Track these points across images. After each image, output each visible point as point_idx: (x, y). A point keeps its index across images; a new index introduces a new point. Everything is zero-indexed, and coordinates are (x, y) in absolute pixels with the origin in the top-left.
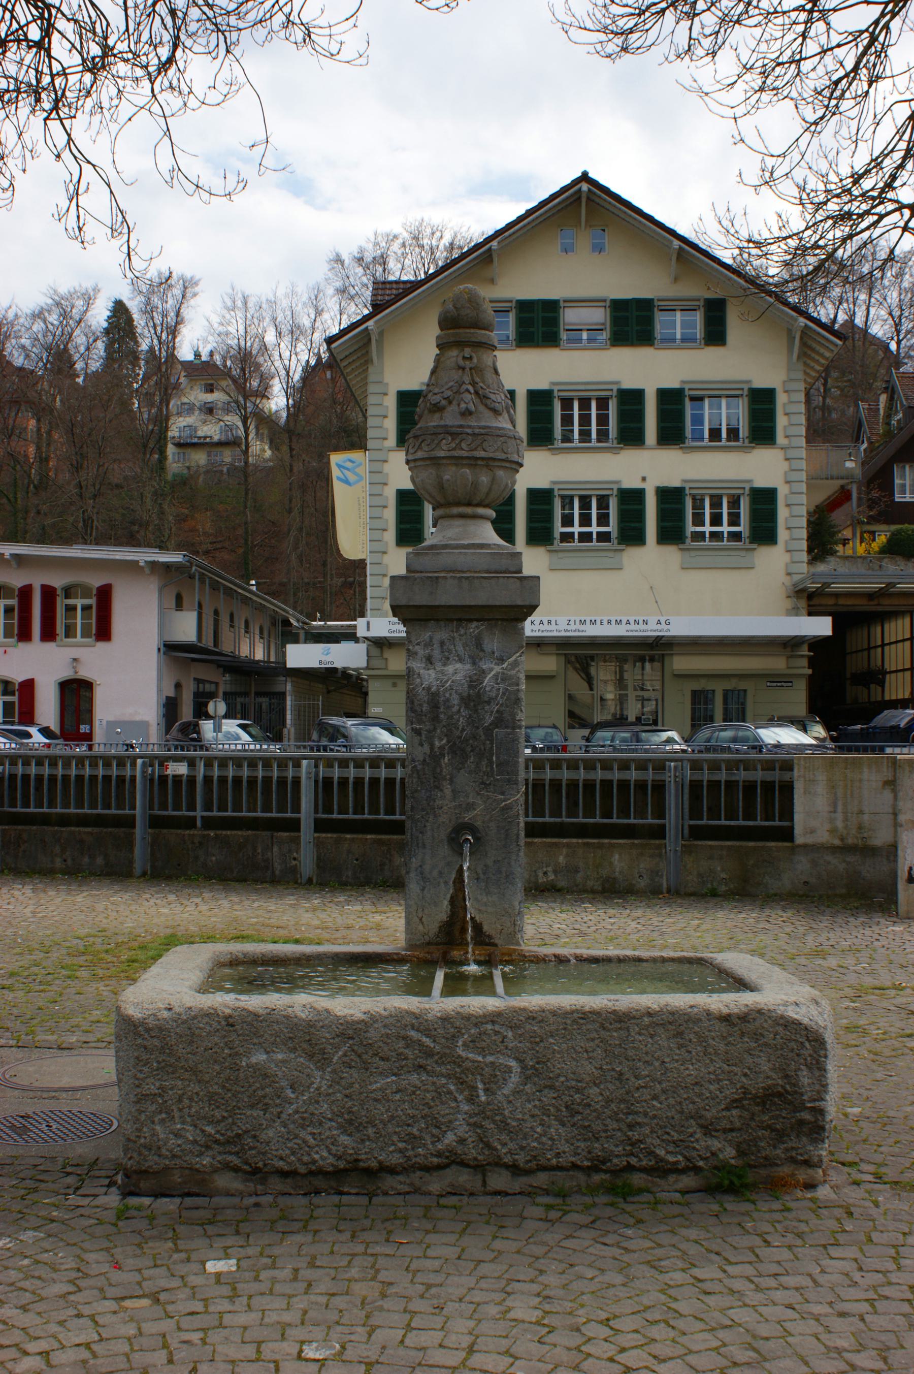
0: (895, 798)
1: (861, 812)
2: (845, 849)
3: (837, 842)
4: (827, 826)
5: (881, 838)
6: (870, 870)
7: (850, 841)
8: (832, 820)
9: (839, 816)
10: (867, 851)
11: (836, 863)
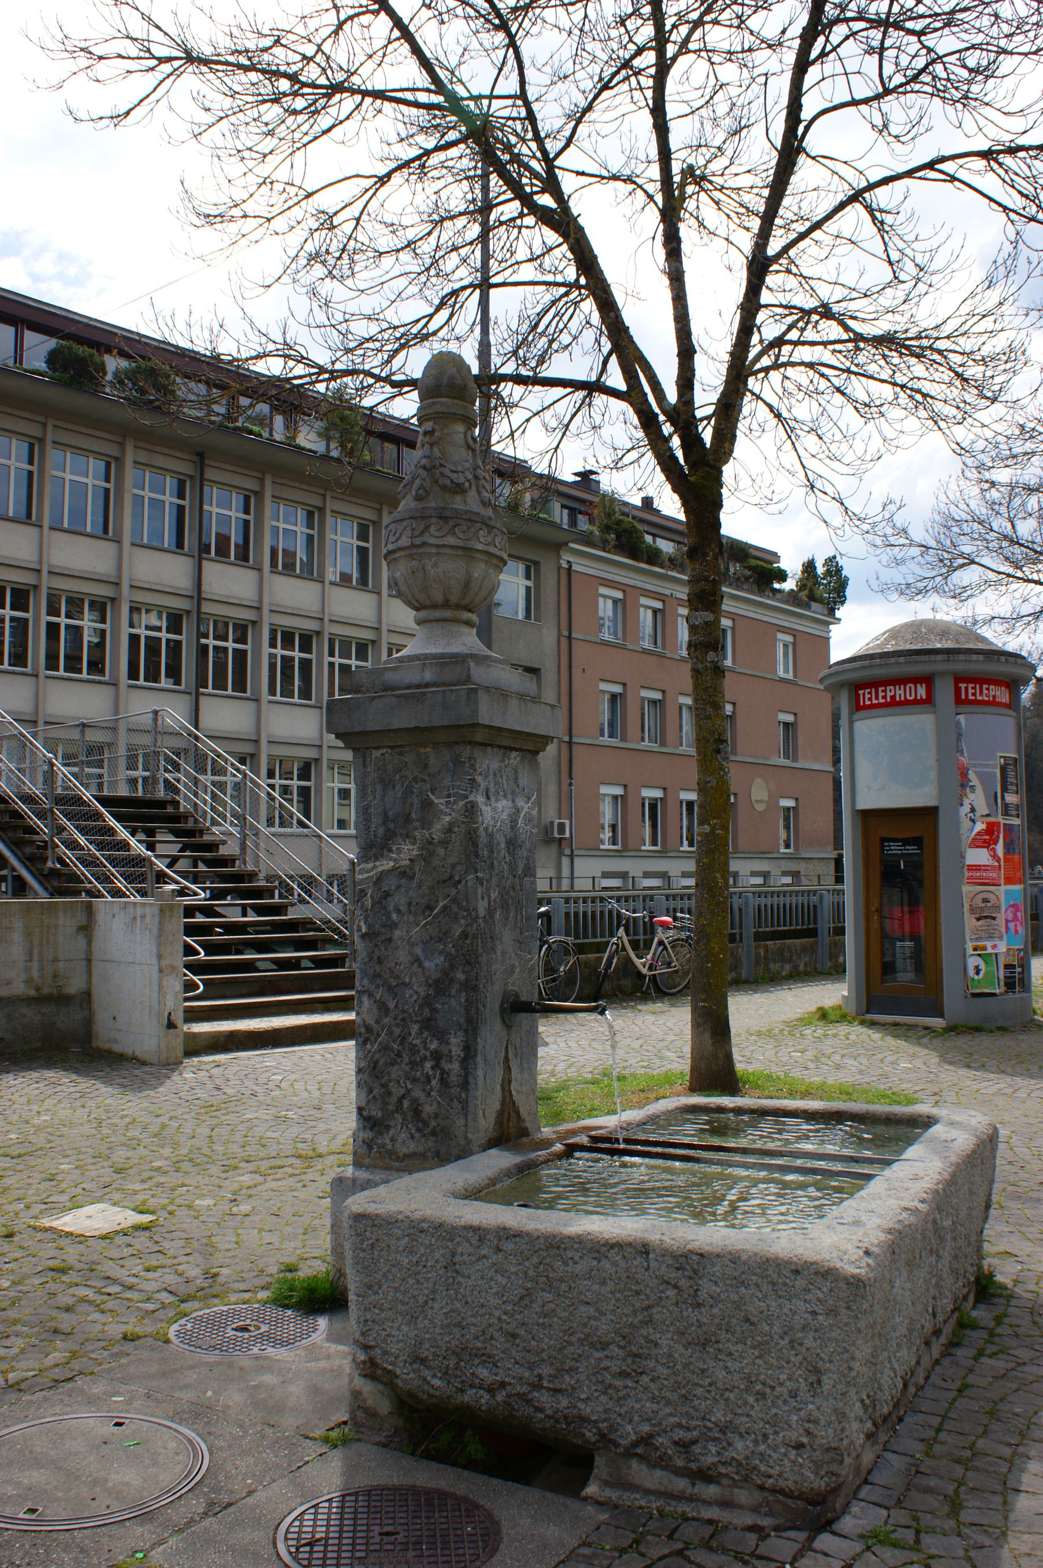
0: (89, 942)
1: (56, 960)
2: (40, 1000)
3: (33, 993)
4: (23, 976)
5: (75, 986)
6: (66, 1020)
7: (46, 991)
8: (27, 970)
9: (35, 965)
10: (62, 1000)
11: (31, 1015)
